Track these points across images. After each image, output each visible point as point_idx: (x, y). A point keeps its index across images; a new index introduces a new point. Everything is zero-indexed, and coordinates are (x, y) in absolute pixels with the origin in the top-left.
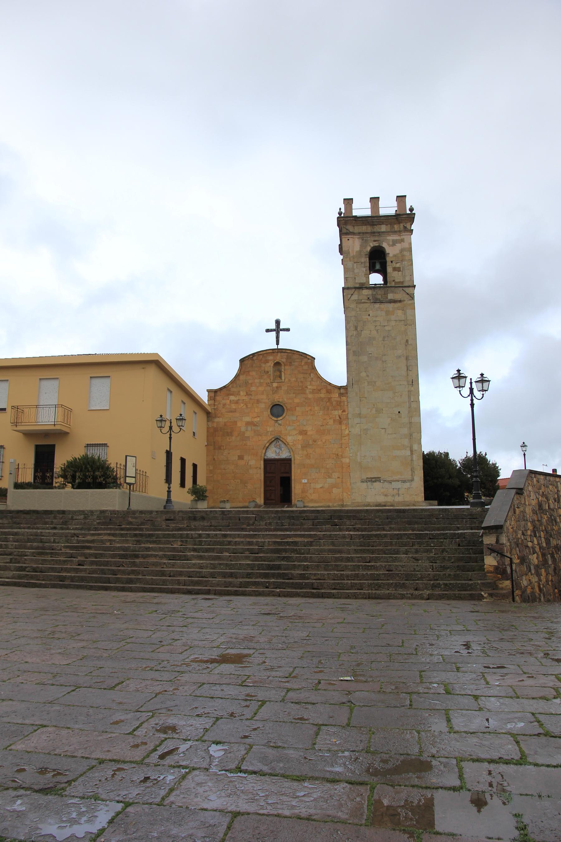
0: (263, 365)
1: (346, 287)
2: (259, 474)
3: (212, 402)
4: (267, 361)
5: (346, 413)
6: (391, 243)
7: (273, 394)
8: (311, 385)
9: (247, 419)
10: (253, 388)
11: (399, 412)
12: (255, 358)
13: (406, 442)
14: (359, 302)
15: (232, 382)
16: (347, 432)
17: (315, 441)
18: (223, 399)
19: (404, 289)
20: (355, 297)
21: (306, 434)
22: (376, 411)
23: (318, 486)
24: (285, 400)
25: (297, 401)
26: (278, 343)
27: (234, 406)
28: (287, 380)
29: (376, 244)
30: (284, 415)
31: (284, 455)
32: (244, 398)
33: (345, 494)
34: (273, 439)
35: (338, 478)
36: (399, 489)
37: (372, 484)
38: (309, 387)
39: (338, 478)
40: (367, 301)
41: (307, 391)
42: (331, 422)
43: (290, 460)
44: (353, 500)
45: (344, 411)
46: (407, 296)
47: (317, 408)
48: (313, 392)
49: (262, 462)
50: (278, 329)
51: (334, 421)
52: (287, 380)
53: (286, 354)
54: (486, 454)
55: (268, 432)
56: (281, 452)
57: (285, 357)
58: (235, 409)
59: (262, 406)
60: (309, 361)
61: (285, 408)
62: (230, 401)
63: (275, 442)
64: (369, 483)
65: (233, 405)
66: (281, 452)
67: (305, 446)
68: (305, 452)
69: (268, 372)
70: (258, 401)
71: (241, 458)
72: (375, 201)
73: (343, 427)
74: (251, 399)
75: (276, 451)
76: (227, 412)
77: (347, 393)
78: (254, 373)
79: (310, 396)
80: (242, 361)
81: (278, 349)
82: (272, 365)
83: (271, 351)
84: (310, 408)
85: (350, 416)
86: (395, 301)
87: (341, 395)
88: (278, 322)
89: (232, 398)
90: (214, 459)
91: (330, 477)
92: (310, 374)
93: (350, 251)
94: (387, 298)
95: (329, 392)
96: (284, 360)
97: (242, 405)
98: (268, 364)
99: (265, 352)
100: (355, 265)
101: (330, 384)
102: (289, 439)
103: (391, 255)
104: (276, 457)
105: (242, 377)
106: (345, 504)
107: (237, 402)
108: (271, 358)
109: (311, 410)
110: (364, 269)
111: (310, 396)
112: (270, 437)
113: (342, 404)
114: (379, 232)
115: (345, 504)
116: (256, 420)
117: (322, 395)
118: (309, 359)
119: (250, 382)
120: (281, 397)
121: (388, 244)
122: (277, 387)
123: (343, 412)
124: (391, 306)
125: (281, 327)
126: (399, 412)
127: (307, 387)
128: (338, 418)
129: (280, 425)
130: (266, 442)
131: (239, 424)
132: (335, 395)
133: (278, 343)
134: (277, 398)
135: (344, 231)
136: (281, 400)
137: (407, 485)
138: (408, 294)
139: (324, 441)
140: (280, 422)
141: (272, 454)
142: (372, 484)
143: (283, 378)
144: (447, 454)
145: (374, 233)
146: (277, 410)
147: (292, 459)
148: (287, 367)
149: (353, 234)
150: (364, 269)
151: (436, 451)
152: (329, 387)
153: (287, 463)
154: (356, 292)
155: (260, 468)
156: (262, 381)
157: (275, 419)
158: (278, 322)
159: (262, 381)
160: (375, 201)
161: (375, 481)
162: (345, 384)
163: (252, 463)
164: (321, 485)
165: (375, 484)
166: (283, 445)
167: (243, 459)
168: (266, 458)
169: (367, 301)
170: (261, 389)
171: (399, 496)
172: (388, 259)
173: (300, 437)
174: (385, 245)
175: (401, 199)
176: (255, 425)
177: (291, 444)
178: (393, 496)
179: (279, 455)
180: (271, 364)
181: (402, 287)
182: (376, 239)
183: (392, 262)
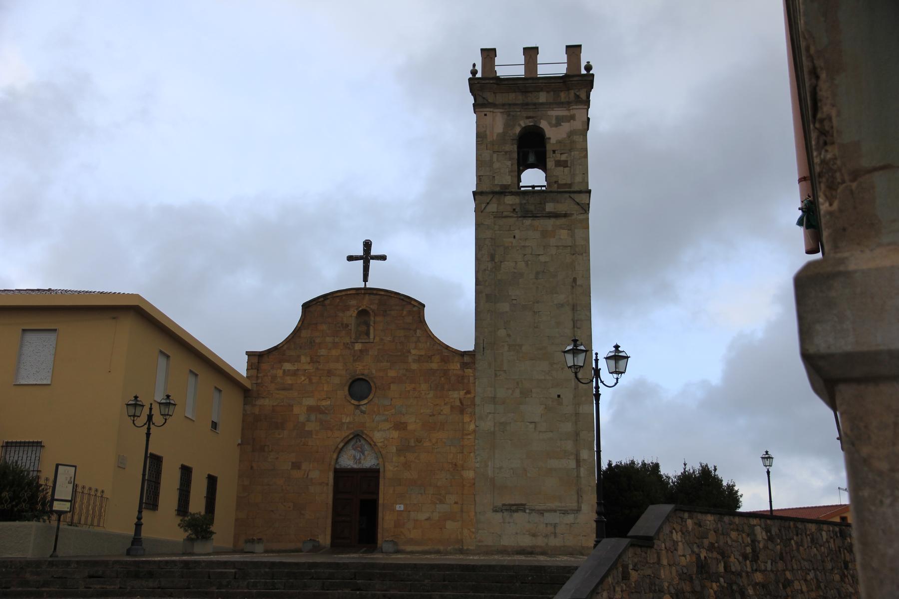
0: (341, 314)
1: (479, 190)
2: (323, 495)
3: (254, 372)
4: (347, 308)
5: (472, 395)
6: (554, 122)
7: (354, 361)
8: (415, 348)
9: (310, 402)
10: (323, 352)
11: (559, 396)
12: (327, 302)
13: (569, 445)
14: (499, 216)
15: (288, 340)
16: (472, 427)
17: (419, 440)
18: (273, 368)
19: (572, 195)
20: (493, 207)
21: (405, 428)
22: (521, 393)
23: (422, 516)
24: (374, 371)
25: (392, 373)
26: (365, 279)
27: (289, 380)
28: (377, 339)
29: (530, 123)
30: (371, 397)
31: (369, 462)
32: (307, 367)
33: (466, 532)
34: (351, 436)
35: (456, 503)
36: (555, 526)
37: (511, 516)
38: (413, 352)
39: (456, 503)
40: (512, 214)
41: (410, 359)
42: (446, 410)
43: (378, 471)
44: (480, 541)
45: (468, 392)
46: (576, 207)
47: (424, 386)
48: (419, 359)
49: (331, 475)
50: (367, 256)
51: (452, 408)
52: (377, 339)
53: (378, 297)
54: (715, 470)
55: (343, 424)
56: (363, 457)
57: (377, 302)
58: (292, 385)
59: (336, 380)
60: (415, 309)
61: (372, 384)
62: (284, 371)
63: (354, 441)
64: (506, 514)
65: (288, 378)
66: (363, 457)
67: (403, 449)
68: (402, 459)
69: (347, 326)
70: (330, 373)
71: (296, 466)
72: (531, 53)
73: (467, 419)
74: (317, 369)
75: (354, 456)
76: (278, 389)
77: (474, 363)
78: (324, 327)
79: (414, 366)
80: (306, 306)
81: (365, 289)
82: (355, 314)
83: (354, 292)
84: (413, 385)
85: (478, 400)
86: (556, 216)
87: (464, 365)
88: (367, 245)
89: (287, 366)
90: (252, 467)
91: (441, 502)
92: (415, 331)
93: (488, 133)
94: (544, 209)
95: (445, 360)
96: (374, 307)
97: (303, 378)
98: (348, 313)
99: (343, 293)
100: (495, 156)
101: (447, 347)
102: (378, 436)
103: (553, 141)
104: (355, 466)
105: (304, 334)
106: (465, 548)
107: (295, 373)
108: (353, 302)
109: (414, 389)
110: (509, 163)
111: (414, 366)
112: (345, 433)
113: (466, 381)
114: (535, 104)
115: (465, 548)
116: (324, 403)
117: (434, 366)
118: (414, 306)
119: (318, 340)
120: (366, 367)
121: (550, 124)
122: (361, 351)
123: (466, 393)
124: (550, 223)
125: (374, 252)
126: (559, 396)
127: (409, 352)
128: (458, 403)
129: (363, 412)
130: (339, 440)
131: (296, 410)
132: (455, 367)
133: (365, 279)
134: (360, 367)
135: (480, 101)
136: (366, 372)
137: (570, 518)
138: (578, 204)
139: (434, 441)
140: (363, 408)
141: (347, 461)
142: (511, 516)
143: (372, 336)
144: (656, 466)
145: (527, 104)
146: (359, 388)
147: (381, 470)
148: (378, 319)
149: (494, 105)
150: (509, 163)
151: (639, 461)
152: (446, 353)
153: (372, 476)
154: (494, 200)
155: (327, 484)
156: (337, 340)
157: (356, 403)
158: (367, 245)
159: (337, 340)
160: (531, 53)
161: (517, 511)
162: (471, 347)
163: (315, 474)
164: (427, 515)
165: (515, 515)
166: (366, 447)
167: (299, 468)
168: (338, 467)
169: (512, 214)
170: (334, 353)
171: (555, 536)
172: (549, 148)
173: (395, 434)
174: (544, 125)
175: (573, 51)
176: (322, 412)
177: (379, 445)
178: (546, 536)
179: (360, 463)
180: (354, 313)
181: (570, 192)
182: (531, 114)
183: (554, 152)
